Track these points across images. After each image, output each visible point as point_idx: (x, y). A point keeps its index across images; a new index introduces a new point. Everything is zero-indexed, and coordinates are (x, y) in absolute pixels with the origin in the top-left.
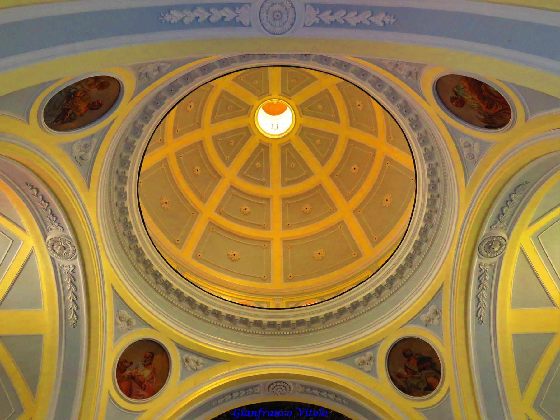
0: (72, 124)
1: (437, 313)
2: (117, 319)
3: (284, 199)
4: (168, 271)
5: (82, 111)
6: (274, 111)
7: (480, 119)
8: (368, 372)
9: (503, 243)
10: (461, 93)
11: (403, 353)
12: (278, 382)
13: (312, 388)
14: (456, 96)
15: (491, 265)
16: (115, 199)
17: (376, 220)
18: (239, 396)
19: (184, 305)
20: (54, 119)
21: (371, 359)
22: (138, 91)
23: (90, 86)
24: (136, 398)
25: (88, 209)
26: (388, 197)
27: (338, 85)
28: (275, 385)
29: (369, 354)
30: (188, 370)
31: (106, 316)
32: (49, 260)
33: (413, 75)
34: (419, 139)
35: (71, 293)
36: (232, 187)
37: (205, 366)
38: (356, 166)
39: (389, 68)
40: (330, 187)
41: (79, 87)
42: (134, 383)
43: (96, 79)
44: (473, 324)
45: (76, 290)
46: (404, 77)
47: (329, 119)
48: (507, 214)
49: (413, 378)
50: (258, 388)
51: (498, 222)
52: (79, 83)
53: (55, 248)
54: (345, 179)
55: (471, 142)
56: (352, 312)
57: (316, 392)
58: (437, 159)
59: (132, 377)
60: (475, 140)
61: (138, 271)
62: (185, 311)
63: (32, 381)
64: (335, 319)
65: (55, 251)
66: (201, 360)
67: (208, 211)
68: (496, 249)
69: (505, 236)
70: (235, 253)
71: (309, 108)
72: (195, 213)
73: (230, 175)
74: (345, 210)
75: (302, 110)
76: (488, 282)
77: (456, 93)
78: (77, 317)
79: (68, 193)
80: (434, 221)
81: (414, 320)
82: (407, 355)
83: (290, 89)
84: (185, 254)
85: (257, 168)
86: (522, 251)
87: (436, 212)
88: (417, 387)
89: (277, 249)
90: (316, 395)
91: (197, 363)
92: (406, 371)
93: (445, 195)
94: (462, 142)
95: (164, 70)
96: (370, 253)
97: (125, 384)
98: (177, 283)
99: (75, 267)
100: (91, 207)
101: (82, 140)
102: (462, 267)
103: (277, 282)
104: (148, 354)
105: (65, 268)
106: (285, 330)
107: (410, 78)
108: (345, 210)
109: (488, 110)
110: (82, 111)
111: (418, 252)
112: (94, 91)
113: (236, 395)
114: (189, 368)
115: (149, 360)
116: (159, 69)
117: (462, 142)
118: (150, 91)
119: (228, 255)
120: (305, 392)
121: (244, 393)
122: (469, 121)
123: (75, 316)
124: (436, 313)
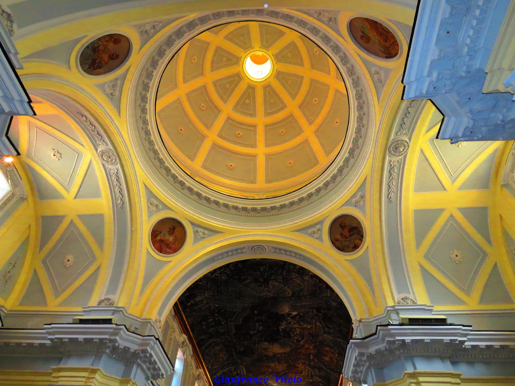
0: (101, 70)
1: (362, 197)
5: (106, 60)
6: (259, 61)
7: (381, 51)
8: (317, 238)
9: (406, 145)
10: (366, 31)
11: (340, 225)
12: (257, 246)
13: (280, 250)
14: (363, 34)
15: (398, 161)
16: (141, 125)
18: (232, 255)
20: (87, 67)
21: (319, 230)
22: (143, 44)
23: (107, 41)
25: (121, 131)
27: (300, 37)
28: (255, 247)
29: (318, 226)
31: (141, 203)
32: (101, 165)
33: (332, 21)
35: (117, 187)
36: (228, 117)
37: (209, 236)
38: (316, 99)
39: (315, 16)
40: (298, 114)
41: (100, 43)
43: (111, 36)
44: (385, 202)
46: (326, 22)
47: (297, 64)
48: (408, 124)
50: (244, 249)
51: (402, 129)
52: (99, 39)
53: (103, 157)
54: (308, 107)
55: (379, 70)
57: (282, 252)
59: (162, 241)
60: (381, 68)
62: (195, 201)
63: (100, 243)
65: (104, 159)
66: (206, 232)
67: (212, 137)
68: (401, 149)
69: (408, 141)
70: (231, 164)
71: (282, 57)
72: (203, 137)
73: (227, 109)
74: (308, 132)
75: (279, 58)
76: (396, 174)
77: (363, 32)
79: (107, 121)
80: (362, 133)
81: (347, 203)
82: (343, 226)
83: (267, 42)
85: (246, 104)
86: (422, 151)
87: (363, 126)
88: (348, 247)
91: (204, 233)
92: (342, 237)
94: (373, 70)
95: (157, 28)
96: (324, 161)
98: (189, 182)
100: (123, 129)
101: (111, 82)
102: (378, 164)
105: (112, 171)
107: (331, 23)
109: (385, 44)
110: (106, 60)
112: (111, 45)
113: (230, 253)
114: (198, 237)
115: (172, 231)
116: (154, 27)
117: (373, 70)
120: (276, 252)
121: (235, 252)
122: (375, 54)
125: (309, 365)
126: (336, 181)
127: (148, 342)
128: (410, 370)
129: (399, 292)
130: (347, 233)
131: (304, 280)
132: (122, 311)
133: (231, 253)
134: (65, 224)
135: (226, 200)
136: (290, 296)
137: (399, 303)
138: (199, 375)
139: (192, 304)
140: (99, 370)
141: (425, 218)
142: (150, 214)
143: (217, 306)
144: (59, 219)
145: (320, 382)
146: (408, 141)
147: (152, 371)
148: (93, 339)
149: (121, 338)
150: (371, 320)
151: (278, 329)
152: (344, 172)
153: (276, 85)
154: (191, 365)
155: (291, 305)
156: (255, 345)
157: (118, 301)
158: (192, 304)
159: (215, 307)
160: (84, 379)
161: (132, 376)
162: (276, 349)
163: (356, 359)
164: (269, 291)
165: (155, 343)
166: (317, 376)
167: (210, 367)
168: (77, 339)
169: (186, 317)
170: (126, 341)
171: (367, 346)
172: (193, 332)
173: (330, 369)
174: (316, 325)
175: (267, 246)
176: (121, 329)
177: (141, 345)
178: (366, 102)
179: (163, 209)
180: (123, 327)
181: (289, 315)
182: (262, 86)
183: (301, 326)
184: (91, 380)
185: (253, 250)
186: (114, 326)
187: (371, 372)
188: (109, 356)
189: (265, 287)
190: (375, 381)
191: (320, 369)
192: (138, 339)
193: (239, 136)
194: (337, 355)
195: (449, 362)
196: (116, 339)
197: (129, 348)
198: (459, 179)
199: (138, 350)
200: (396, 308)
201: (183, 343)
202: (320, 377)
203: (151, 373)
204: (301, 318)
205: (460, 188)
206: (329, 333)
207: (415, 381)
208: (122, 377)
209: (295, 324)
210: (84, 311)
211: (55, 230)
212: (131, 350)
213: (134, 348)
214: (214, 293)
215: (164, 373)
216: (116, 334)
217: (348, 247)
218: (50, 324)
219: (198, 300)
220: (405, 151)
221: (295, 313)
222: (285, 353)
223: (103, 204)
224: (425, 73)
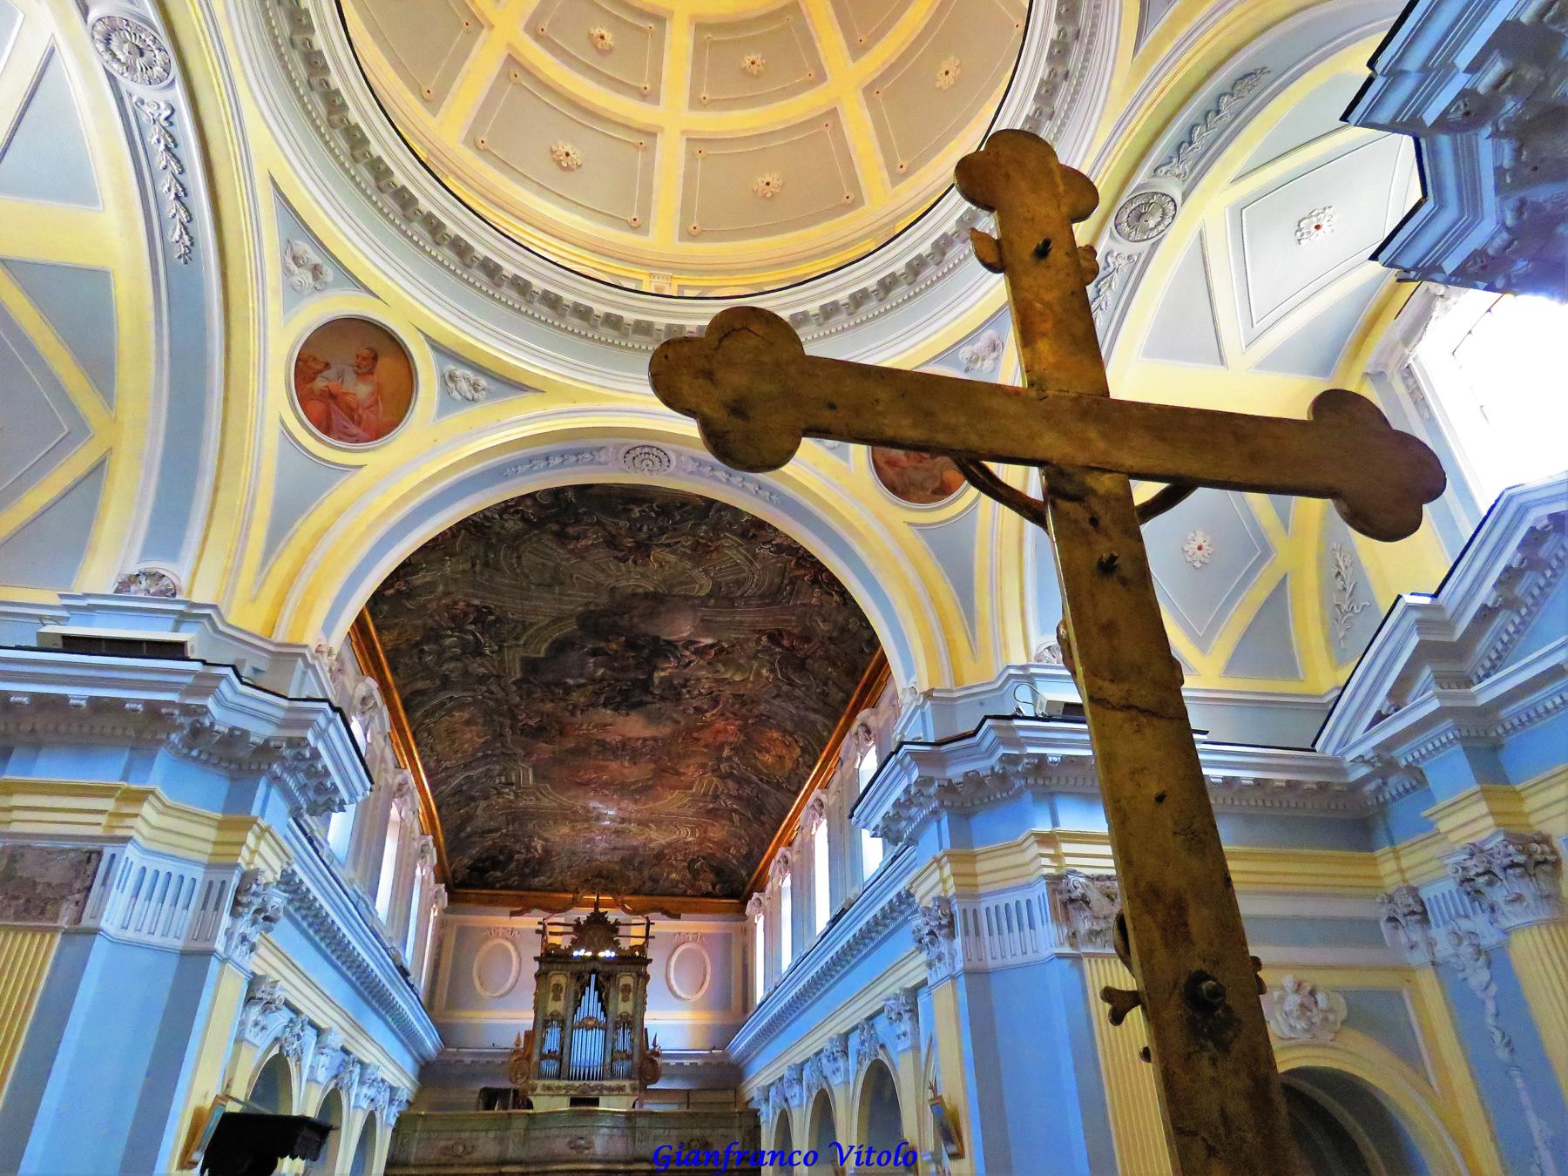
2: (290, 261)
3: (701, 26)
4: (410, 167)
9: (1167, 208)
15: (1129, 257)
18: (561, 465)
19: (446, 254)
24: (340, 439)
26: (951, 63)
30: (451, 399)
35: (168, 176)
37: (492, 395)
42: (333, 406)
45: (182, 172)
49: (916, 468)
53: (114, 45)
61: (332, 151)
65: (114, 55)
66: (483, 382)
68: (1152, 223)
69: (1178, 200)
74: (845, 79)
78: (191, 239)
84: (446, 129)
89: (670, 158)
90: (719, 480)
91: (475, 387)
93: (1081, 76)
97: (318, 407)
98: (429, 198)
99: (173, 111)
103: (662, 237)
104: (365, 353)
108: (845, 79)
114: (455, 394)
115: (366, 366)
119: (552, 152)
121: (573, 459)
123: (186, 237)
124: (994, 347)
125: (715, 770)
126: (920, 277)
127: (312, 716)
128: (1044, 827)
131: (755, 556)
132: (209, 616)
133: (558, 460)
136: (703, 593)
138: (401, 785)
139: (399, 592)
140: (152, 792)
142: (293, 294)
143: (477, 602)
145: (735, 811)
147: (311, 794)
148: (122, 702)
149: (218, 702)
150: (956, 695)
151: (651, 677)
152: (949, 255)
154: (383, 760)
155: (703, 620)
156: (573, 714)
157: (192, 584)
158: (399, 592)
159: (468, 605)
160: (102, 819)
161: (255, 811)
162: (634, 726)
163: (907, 791)
164: (644, 576)
165: (330, 721)
166: (730, 796)
167: (432, 764)
168: (65, 698)
169: (378, 629)
170: (227, 709)
171: (942, 762)
172: (394, 670)
173: (768, 783)
174: (758, 674)
175: (675, 451)
176: (222, 677)
177: (284, 724)
179: (336, 284)
180: (229, 671)
181: (689, 643)
183: (717, 676)
184: (128, 822)
185: (630, 457)
186: (197, 666)
187: (939, 822)
188: (177, 753)
189: (635, 562)
191: (741, 781)
192: (276, 707)
193: (600, 43)
194: (798, 750)
196: (205, 706)
197: (245, 733)
199: (276, 739)
200: (1033, 670)
201: (364, 701)
202: (738, 798)
203: (308, 800)
204: (721, 654)
205: (1261, 366)
206: (789, 697)
207: (1052, 852)
208: (224, 811)
209: (702, 668)
212: (252, 739)
213: (260, 731)
214: (474, 565)
215: (346, 798)
216: (206, 692)
217: (923, 488)
219: (419, 582)
220: (1161, 228)
221: (709, 641)
222: (655, 739)
223: (108, 233)
224: (1464, 58)
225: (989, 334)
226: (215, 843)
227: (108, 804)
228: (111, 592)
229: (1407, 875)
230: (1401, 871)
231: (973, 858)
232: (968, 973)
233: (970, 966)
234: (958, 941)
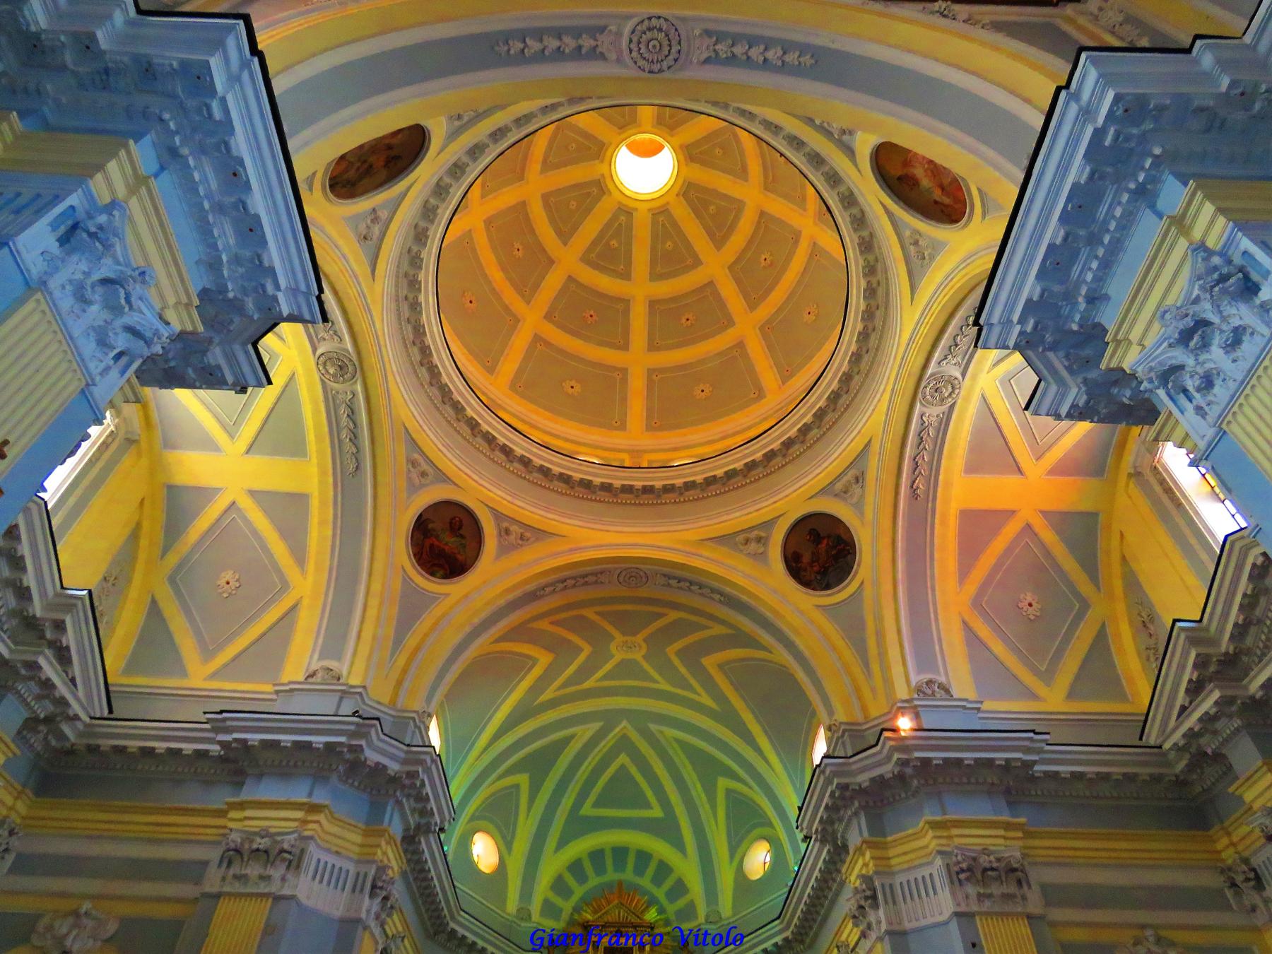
17: (786, 340)
30: (504, 549)
34: (860, 245)
54: (753, 276)
56: (745, 476)
58: (880, 276)
64: (698, 491)
75: (690, 154)
82: (815, 537)
106: (645, 499)
111: (832, 407)
118: (468, 139)
127: (423, 757)
129: (919, 672)
130: (821, 553)
132: (360, 694)
134: (220, 504)
135: (626, 478)
137: (919, 690)
141: (979, 525)
144: (205, 494)
146: (960, 377)
153: (682, 212)
176: (374, 726)
177: (405, 762)
178: (883, 283)
182: (649, 210)
190: (866, 834)
195: (1004, 803)
197: (385, 767)
198: (1048, 455)
210: (277, 692)
211: (195, 515)
213: (394, 767)
218: (221, 712)
224: (1015, 318)
225: (430, 470)
226: (362, 846)
227: (299, 814)
228: (301, 679)
229: (1240, 848)
230: (1233, 844)
231: (884, 846)
232: (889, 933)
233: (891, 928)
234: (881, 912)
